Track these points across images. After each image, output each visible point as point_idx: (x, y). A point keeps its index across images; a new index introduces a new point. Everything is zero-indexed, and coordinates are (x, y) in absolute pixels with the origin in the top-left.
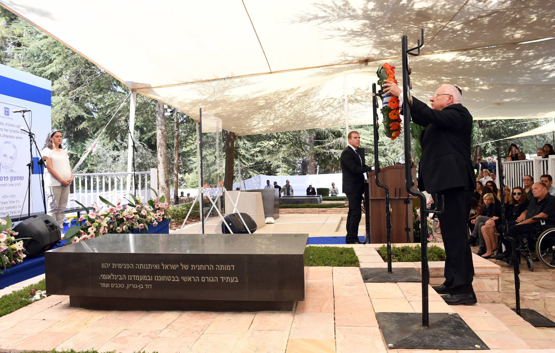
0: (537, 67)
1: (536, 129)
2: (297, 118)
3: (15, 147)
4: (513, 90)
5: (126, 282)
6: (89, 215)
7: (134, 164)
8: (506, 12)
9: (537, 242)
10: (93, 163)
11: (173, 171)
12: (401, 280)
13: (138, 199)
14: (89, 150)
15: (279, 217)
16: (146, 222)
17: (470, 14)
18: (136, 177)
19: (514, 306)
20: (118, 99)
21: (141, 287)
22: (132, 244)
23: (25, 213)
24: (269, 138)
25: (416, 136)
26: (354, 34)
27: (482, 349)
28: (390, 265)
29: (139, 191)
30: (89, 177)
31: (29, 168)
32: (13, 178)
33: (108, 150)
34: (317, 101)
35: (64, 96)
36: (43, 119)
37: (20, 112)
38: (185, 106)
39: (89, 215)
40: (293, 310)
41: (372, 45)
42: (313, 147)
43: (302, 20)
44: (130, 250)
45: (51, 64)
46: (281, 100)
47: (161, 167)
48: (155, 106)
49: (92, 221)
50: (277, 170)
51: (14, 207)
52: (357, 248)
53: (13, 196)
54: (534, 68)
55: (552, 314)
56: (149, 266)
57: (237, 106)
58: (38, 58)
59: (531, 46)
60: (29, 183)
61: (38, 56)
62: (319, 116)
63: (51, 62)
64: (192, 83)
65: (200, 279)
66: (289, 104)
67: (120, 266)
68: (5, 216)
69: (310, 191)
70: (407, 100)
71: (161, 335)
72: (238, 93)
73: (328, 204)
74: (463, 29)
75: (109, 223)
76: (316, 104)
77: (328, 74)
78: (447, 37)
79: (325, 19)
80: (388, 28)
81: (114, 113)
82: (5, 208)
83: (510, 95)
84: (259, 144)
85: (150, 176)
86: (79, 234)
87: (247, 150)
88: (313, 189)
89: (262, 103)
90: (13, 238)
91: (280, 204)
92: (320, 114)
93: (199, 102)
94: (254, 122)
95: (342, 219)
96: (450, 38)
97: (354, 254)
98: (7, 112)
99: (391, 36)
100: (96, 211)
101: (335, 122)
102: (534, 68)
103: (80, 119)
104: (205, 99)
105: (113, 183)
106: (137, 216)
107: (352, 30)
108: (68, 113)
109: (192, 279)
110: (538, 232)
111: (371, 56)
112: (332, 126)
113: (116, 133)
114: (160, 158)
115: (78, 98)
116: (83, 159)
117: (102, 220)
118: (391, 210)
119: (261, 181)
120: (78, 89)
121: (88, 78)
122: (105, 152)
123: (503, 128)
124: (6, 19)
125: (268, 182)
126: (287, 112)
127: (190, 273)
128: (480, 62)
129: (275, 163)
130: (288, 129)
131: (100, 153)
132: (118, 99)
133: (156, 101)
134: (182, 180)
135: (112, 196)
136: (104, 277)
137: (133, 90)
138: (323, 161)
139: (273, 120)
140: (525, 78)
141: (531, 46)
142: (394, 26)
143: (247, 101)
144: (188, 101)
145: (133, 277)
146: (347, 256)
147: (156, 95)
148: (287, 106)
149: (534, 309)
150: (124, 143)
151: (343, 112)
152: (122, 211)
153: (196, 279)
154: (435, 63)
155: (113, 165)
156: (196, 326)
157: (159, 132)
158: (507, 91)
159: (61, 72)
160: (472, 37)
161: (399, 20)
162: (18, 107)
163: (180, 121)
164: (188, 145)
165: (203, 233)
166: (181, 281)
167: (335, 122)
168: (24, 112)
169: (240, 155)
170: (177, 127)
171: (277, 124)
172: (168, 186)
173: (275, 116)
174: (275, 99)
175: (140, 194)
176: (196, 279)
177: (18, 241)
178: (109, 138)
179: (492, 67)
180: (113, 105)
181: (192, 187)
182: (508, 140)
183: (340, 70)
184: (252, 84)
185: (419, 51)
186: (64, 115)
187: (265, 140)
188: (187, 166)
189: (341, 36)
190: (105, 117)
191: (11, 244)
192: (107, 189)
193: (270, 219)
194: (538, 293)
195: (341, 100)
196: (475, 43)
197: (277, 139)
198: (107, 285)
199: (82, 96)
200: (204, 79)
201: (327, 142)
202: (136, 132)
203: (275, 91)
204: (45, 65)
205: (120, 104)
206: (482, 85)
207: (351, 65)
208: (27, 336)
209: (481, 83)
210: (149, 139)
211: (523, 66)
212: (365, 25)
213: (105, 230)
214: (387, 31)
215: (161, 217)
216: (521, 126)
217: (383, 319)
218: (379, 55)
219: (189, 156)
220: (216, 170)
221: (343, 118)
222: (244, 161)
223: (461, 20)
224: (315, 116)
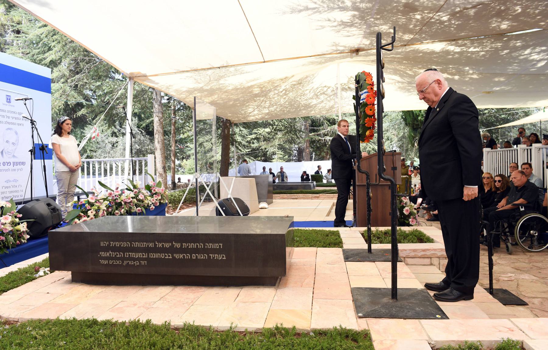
0: (525, 57)
1: (527, 118)
2: (291, 105)
3: (16, 133)
4: (502, 79)
5: (123, 259)
6: (89, 199)
7: (131, 150)
8: (491, 4)
9: (516, 227)
10: (92, 149)
11: (170, 157)
12: (379, 260)
13: (135, 183)
14: (88, 136)
15: (272, 202)
16: (144, 206)
17: (456, 6)
18: (134, 164)
19: (488, 286)
20: (116, 87)
21: (137, 263)
22: (130, 225)
23: (28, 197)
24: (265, 125)
25: (409, 124)
26: (344, 24)
27: (442, 318)
28: (370, 247)
29: (137, 177)
30: (88, 163)
31: (31, 154)
32: (14, 164)
33: (106, 137)
34: (311, 90)
35: (63, 83)
36: (44, 107)
37: (22, 100)
38: (181, 94)
39: (89, 199)
40: (277, 285)
41: (362, 36)
42: (306, 134)
43: (293, 11)
44: (128, 229)
45: (51, 52)
46: (275, 88)
47: (158, 153)
48: (152, 93)
49: (92, 205)
50: (273, 157)
51: (16, 191)
52: (342, 231)
53: (15, 181)
54: (522, 57)
55: (523, 293)
56: (145, 245)
57: (232, 94)
58: (38, 45)
59: (518, 37)
60: (32, 168)
61: (37, 43)
62: (313, 103)
63: (50, 49)
64: (187, 71)
65: (191, 257)
66: (284, 92)
67: (117, 244)
68: (9, 199)
69: (305, 177)
70: (380, 92)
71: (155, 306)
72: (233, 81)
73: (321, 191)
74: (449, 20)
75: (108, 207)
76: (310, 92)
77: (320, 63)
78: (434, 27)
79: (315, 10)
80: (377, 19)
81: (112, 100)
82: (8, 193)
83: (499, 84)
84: (255, 131)
85: (147, 163)
86: (79, 217)
87: (244, 137)
88: (308, 175)
89: (257, 91)
90: (17, 220)
91: (274, 189)
92: (314, 102)
93: (195, 90)
94: (250, 109)
95: (333, 205)
96: (438, 29)
97: (339, 237)
98: (9, 100)
99: (380, 27)
100: (96, 195)
101: (329, 110)
102: (522, 57)
103: (79, 106)
104: (202, 88)
105: (111, 169)
106: (135, 200)
107: (342, 21)
108: (67, 100)
109: (184, 256)
110: (517, 218)
111: (362, 46)
112: (326, 113)
113: (114, 119)
114: (157, 145)
115: (77, 85)
116: (83, 145)
117: (101, 203)
118: (371, 195)
119: (257, 167)
120: (77, 76)
121: (87, 66)
122: (104, 138)
123: (495, 116)
124: (5, 6)
125: (264, 168)
126: (282, 100)
127: (181, 251)
128: (469, 52)
129: (271, 150)
130: (283, 117)
131: (99, 139)
132: (116, 87)
133: (154, 89)
134: (180, 166)
135: (111, 182)
136: (103, 254)
137: (130, 78)
138: (318, 148)
139: (268, 108)
140: (513, 68)
141: (518, 37)
142: (382, 18)
143: (242, 89)
144: (184, 89)
145: (129, 255)
146: (332, 238)
147: (153, 82)
148: (281, 94)
149: (507, 289)
150: (123, 130)
151: (336, 100)
152: (120, 195)
153: (187, 256)
154: (425, 53)
155: (112, 152)
156: (187, 298)
157: (156, 119)
158: (496, 79)
159: (60, 59)
160: (460, 28)
161: (387, 11)
162: (19, 95)
163: (177, 108)
164: (186, 132)
165: (197, 215)
166: (174, 258)
167: (329, 110)
168: (26, 100)
169: (236, 142)
170: (175, 114)
171: (272, 111)
172: (165, 172)
173: (270, 103)
174: (269, 87)
175: (137, 179)
176: (187, 256)
177: (22, 223)
178: (107, 125)
179: (481, 57)
180: (111, 92)
181: (190, 173)
182: (499, 128)
183: (332, 60)
184: (247, 72)
185: (392, 47)
186: (63, 102)
187: (261, 127)
188: (185, 153)
189: (331, 27)
190: (104, 104)
191: (16, 226)
192: (105, 175)
193: (263, 204)
194: (513, 275)
195: (335, 88)
196: (463, 34)
197: (272, 126)
198: (106, 262)
199: (81, 83)
200: (199, 68)
201: (323, 129)
202: (134, 119)
203: (269, 79)
204: (44, 52)
205: (118, 91)
206: (472, 74)
207: (342, 54)
208: (33, 307)
209: (471, 72)
210: (147, 126)
211: (511, 56)
212: (354, 16)
213: (103, 213)
214: (376, 22)
215: (158, 202)
216: (513, 115)
217: (356, 292)
218: (369, 44)
219: (186, 142)
220: (213, 157)
221: (337, 106)
222: (240, 148)
223: (447, 12)
224: (309, 104)
